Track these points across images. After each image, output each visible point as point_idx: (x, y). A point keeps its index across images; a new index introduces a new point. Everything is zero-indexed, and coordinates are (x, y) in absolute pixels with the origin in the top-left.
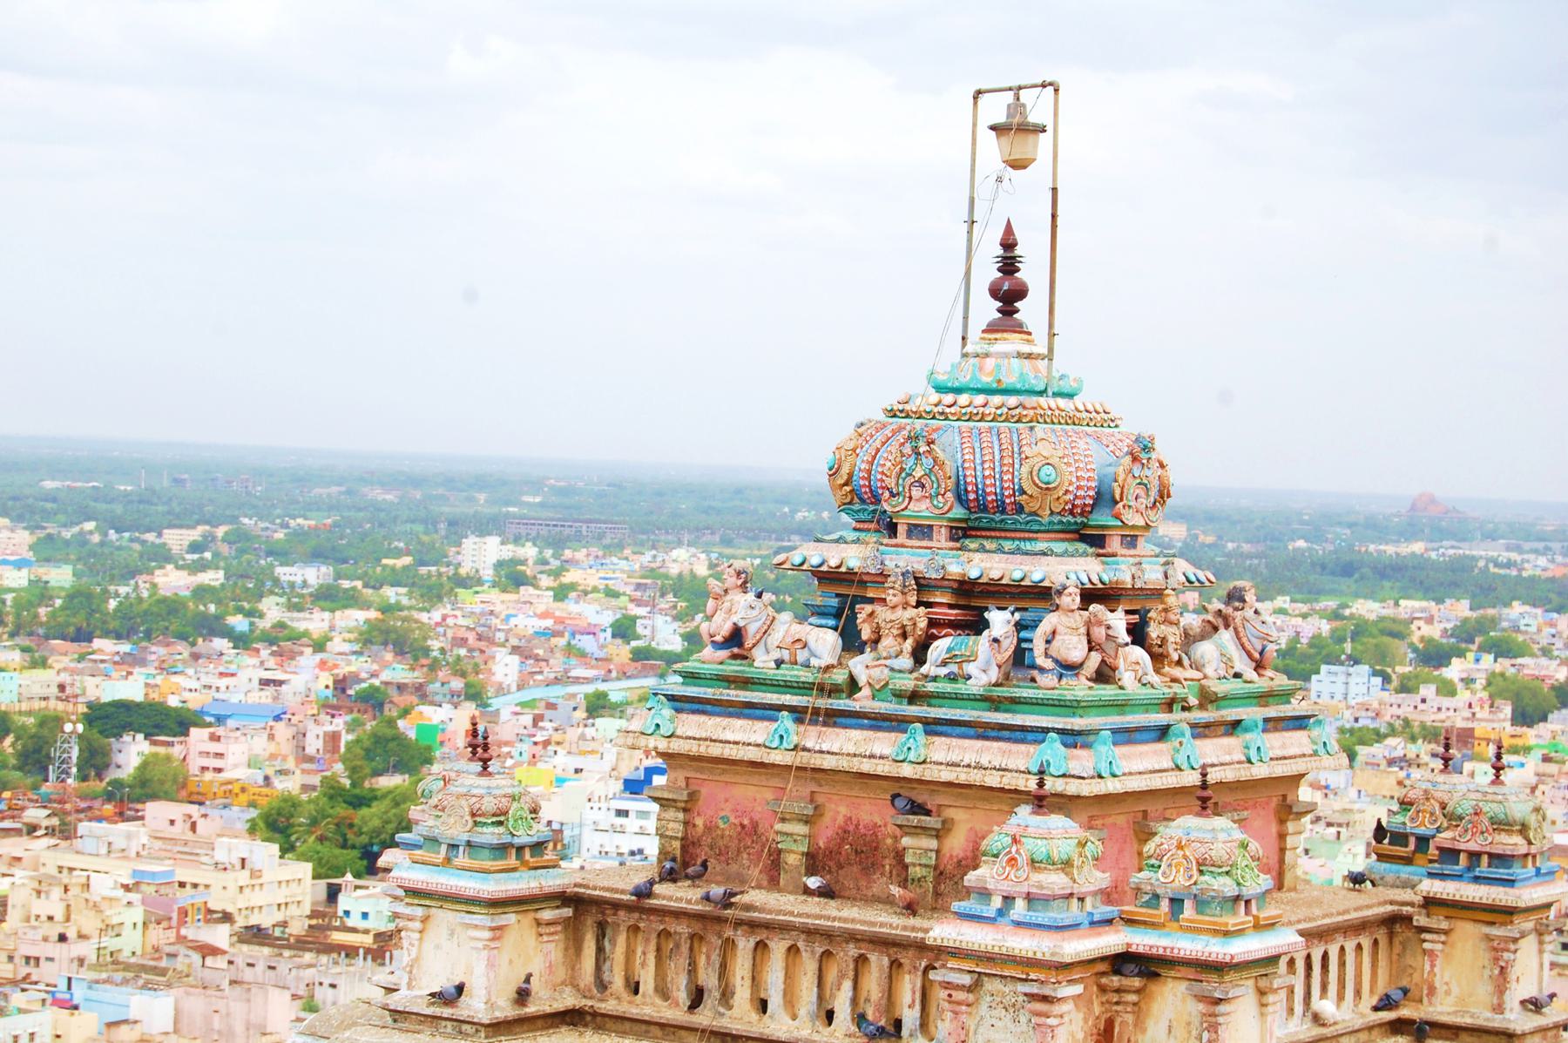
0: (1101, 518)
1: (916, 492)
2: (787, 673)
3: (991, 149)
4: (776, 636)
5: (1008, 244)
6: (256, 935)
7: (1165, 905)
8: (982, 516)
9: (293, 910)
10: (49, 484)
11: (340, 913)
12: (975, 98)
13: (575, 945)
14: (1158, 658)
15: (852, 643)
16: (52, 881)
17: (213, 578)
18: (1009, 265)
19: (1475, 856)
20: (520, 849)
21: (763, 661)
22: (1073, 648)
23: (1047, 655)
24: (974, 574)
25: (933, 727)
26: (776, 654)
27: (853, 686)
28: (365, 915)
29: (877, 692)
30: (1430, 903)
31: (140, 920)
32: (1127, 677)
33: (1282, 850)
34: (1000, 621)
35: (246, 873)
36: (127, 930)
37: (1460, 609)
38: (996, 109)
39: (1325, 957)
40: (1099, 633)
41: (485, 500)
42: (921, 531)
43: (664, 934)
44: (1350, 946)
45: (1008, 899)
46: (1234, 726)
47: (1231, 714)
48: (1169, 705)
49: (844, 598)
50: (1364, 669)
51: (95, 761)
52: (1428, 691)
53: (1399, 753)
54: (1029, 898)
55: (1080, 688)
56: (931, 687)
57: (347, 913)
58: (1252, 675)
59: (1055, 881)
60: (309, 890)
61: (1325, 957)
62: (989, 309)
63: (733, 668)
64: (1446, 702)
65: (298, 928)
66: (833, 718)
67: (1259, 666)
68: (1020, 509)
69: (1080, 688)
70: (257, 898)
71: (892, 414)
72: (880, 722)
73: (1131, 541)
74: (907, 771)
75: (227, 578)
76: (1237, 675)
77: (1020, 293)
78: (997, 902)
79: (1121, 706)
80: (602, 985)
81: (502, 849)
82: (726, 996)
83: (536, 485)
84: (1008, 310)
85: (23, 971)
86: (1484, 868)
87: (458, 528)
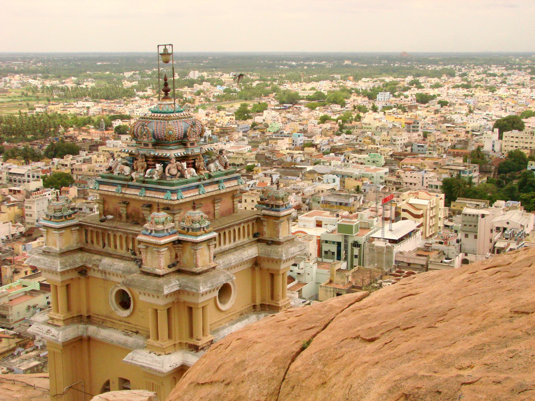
0: (185, 140)
1: (144, 137)
2: (120, 176)
4: (118, 168)
7: (186, 229)
8: (160, 142)
10: (99, 64)
13: (80, 234)
15: (133, 170)
19: (272, 205)
20: (65, 216)
21: (116, 173)
22: (174, 171)
23: (169, 173)
24: (156, 154)
25: (147, 189)
26: (118, 172)
27: (132, 179)
29: (137, 181)
30: (264, 215)
32: (188, 176)
33: (234, 205)
34: (158, 166)
37: (410, 78)
39: (239, 229)
40: (180, 168)
42: (146, 145)
43: (97, 232)
44: (246, 226)
45: (152, 231)
46: (217, 182)
47: (216, 179)
50: (388, 93)
52: (402, 97)
53: (396, 111)
56: (146, 180)
58: (224, 170)
59: (160, 227)
61: (239, 229)
63: (110, 175)
64: (406, 100)
66: (129, 186)
67: (225, 167)
68: (166, 140)
69: (175, 180)
71: (142, 118)
72: (139, 188)
73: (192, 144)
75: (139, 83)
76: (219, 170)
78: (149, 231)
80: (87, 242)
81: (61, 217)
82: (109, 245)
84: (166, 94)
85: (96, 173)
86: (274, 208)
87: (189, 69)
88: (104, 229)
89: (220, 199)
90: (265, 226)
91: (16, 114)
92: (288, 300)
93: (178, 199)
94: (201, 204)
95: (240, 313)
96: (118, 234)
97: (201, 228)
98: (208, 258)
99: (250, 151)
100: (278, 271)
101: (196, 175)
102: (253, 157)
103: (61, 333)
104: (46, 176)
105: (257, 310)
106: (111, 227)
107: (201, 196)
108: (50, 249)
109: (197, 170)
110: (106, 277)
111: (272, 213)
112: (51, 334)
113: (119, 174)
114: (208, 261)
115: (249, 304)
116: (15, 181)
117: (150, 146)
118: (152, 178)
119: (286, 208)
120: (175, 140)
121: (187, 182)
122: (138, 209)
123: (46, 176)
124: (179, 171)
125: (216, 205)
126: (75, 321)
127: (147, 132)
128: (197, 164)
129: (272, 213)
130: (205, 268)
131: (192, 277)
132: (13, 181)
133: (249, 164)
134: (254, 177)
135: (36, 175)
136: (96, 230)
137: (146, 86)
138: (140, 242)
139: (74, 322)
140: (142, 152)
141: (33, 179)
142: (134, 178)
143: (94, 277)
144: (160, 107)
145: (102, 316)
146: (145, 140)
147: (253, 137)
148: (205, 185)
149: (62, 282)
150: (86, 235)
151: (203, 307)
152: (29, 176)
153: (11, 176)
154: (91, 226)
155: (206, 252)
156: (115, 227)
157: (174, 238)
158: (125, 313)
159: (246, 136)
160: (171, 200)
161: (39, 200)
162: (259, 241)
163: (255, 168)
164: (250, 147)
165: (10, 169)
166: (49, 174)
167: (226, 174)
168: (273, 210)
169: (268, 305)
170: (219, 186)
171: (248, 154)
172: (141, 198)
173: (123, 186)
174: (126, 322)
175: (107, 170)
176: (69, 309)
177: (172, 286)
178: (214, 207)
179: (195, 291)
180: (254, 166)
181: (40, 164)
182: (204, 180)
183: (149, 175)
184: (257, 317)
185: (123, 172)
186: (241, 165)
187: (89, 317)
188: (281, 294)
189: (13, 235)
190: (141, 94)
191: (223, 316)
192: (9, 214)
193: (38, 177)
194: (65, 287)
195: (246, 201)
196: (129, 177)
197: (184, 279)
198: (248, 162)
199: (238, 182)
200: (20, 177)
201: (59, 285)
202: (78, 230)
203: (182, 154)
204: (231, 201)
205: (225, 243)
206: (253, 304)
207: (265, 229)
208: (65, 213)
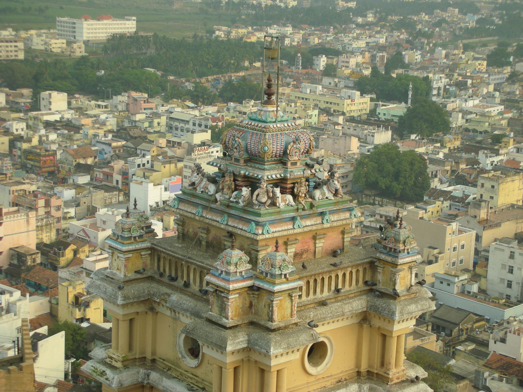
1: (235, 150)
4: (202, 184)
5: (135, 199)
6: (352, 120)
7: (264, 274)
11: (377, 114)
16: (292, 101)
20: (135, 237)
21: (199, 191)
25: (230, 215)
26: (202, 190)
27: (216, 201)
28: (384, 114)
31: (317, 114)
35: (350, 100)
36: (314, 117)
39: (344, 275)
42: (237, 160)
44: (354, 271)
45: (222, 272)
46: (322, 214)
51: (308, 63)
54: (226, 272)
56: (231, 204)
57: (379, 113)
60: (369, 106)
61: (344, 275)
65: (364, 117)
66: (212, 209)
70: (353, 108)
72: (222, 213)
76: (327, 198)
78: (220, 272)
81: (129, 238)
84: (269, 98)
88: (178, 258)
89: (324, 234)
90: (380, 273)
91: (189, 38)
92: (403, 370)
93: (263, 234)
94: (296, 239)
95: (337, 380)
96: (192, 267)
97: (281, 274)
98: (289, 311)
99: (501, 113)
100: (391, 332)
101: (293, 203)
102: (504, 122)
103: (116, 377)
104: (216, 126)
105: (363, 378)
106: (185, 256)
107: (296, 231)
108: (114, 274)
109: (295, 197)
110: (176, 315)
111: (389, 259)
112: (105, 377)
113: (202, 192)
114: (289, 315)
115: (351, 370)
116: (177, 129)
117: (242, 161)
118: (237, 202)
119: (408, 253)
120: (272, 157)
121: (279, 212)
122: (220, 238)
123: (216, 126)
124: (269, 197)
125: (317, 242)
126: (138, 364)
127: (238, 145)
128: (295, 190)
129: (389, 259)
130: (282, 325)
131: (265, 334)
132: (174, 129)
133: (496, 132)
134: (501, 152)
135: (203, 123)
136: (169, 258)
137: (367, 9)
138: (208, 283)
139: (135, 365)
140: (231, 169)
141: (200, 129)
142: (218, 199)
143: (163, 314)
144: (260, 114)
145: (168, 362)
146: (236, 155)
147: (509, 93)
148: (302, 217)
149: (124, 315)
150: (159, 261)
151: (278, 371)
152: (194, 124)
153: (172, 123)
154: (164, 252)
155: (287, 303)
156: (189, 258)
157: (249, 283)
158: (192, 362)
159: (499, 91)
160: (254, 234)
161: (203, 158)
162: (371, 290)
163: (505, 139)
164: (502, 107)
165: (172, 113)
166: (220, 124)
167: (336, 203)
168: (390, 255)
169: (377, 374)
170: (323, 219)
171: (497, 118)
172: (222, 226)
173: (205, 208)
174: (193, 374)
175: (190, 185)
176: (130, 347)
177: (239, 342)
178: (315, 244)
179: (264, 351)
180: (504, 136)
181: (211, 110)
182: (303, 209)
183: (235, 198)
184: (360, 387)
185: (207, 191)
186: (486, 132)
187: (154, 361)
188: (393, 361)
189: (164, 202)
190: (360, 20)
191: (312, 379)
192: (163, 173)
193: (206, 127)
194: (128, 322)
195: (483, 185)
196: (212, 199)
197: (256, 334)
198: (496, 129)
199: (351, 215)
200: (183, 125)
201: (121, 318)
202: (150, 254)
203: (278, 176)
204: (341, 236)
205: (322, 291)
206: (357, 370)
207: (380, 277)
208: (135, 234)
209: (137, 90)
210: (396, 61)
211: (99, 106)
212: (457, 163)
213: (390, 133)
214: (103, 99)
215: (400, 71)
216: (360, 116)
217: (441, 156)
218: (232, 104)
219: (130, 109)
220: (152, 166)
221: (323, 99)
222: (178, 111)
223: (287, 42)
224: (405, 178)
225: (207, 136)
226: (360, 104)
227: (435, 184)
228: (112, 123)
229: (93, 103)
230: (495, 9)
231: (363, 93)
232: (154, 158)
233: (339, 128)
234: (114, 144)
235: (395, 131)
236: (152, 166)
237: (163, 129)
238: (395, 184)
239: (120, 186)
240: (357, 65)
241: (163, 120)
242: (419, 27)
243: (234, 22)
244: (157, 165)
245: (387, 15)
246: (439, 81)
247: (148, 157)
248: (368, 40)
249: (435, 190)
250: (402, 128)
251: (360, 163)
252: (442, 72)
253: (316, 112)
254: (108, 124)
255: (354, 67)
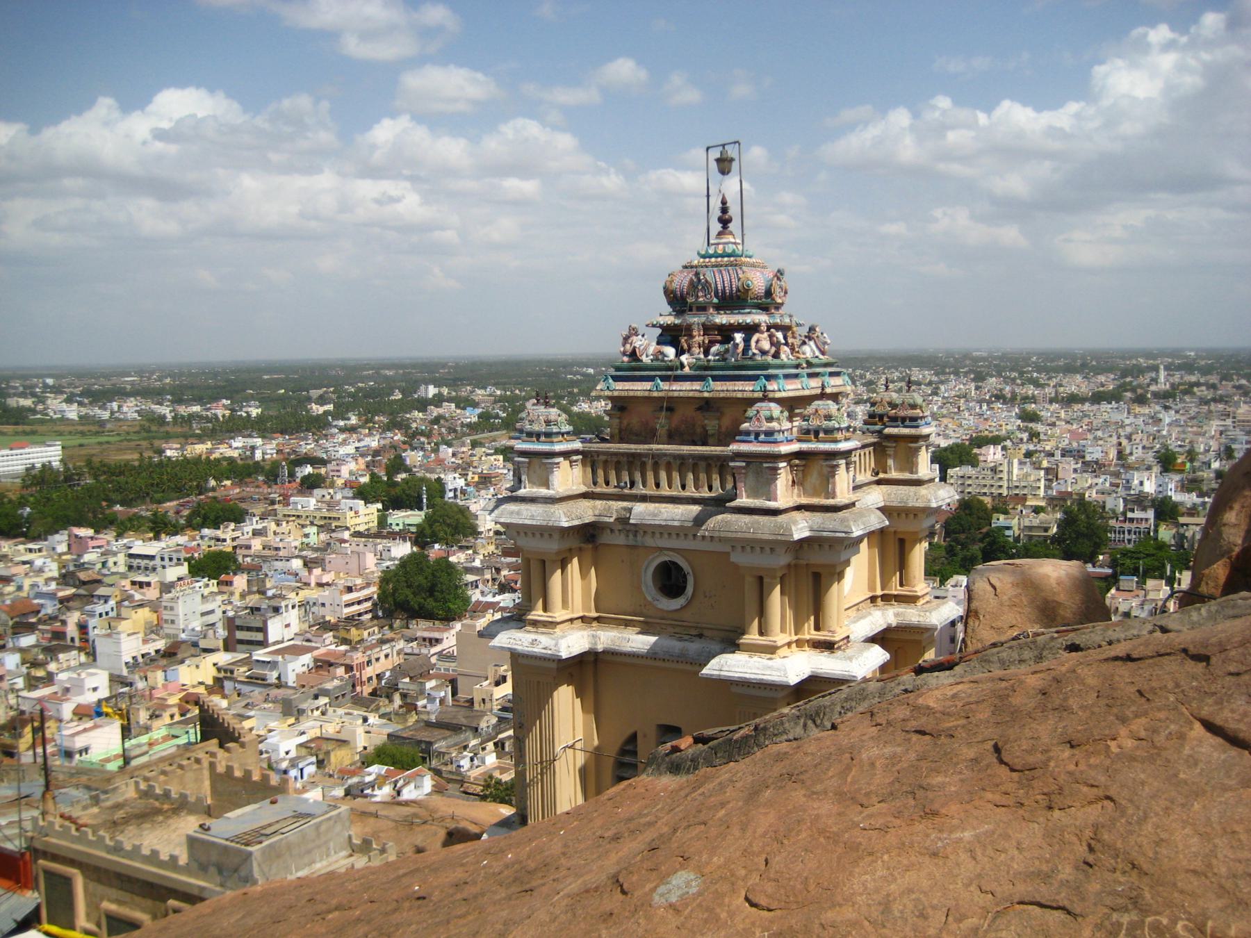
2: (655, 363)
3: (714, 166)
5: (724, 202)
6: (358, 534)
9: (371, 525)
12: (708, 149)
14: (793, 350)
17: (330, 407)
18: (724, 210)
27: (682, 366)
32: (783, 356)
38: (715, 154)
41: (431, 371)
48: (797, 366)
49: (670, 335)
55: (769, 359)
62: (719, 227)
70: (358, 521)
74: (706, 395)
77: (730, 220)
79: (783, 366)
83: (444, 366)
86: (907, 423)
104: (192, 558)
123: (192, 558)
124: (772, 344)
135: (175, 556)
137: (348, 411)
152: (162, 559)
173: (664, 379)
181: (180, 539)
190: (342, 423)
209: (79, 524)
210: (398, 465)
211: (31, 550)
212: (498, 570)
213: (408, 544)
214: (34, 539)
215: (404, 476)
216: (368, 530)
217: (477, 563)
218: (206, 531)
219: (77, 545)
220: (119, 615)
221: (318, 515)
222: (140, 547)
223: (258, 455)
224: (442, 592)
225: (184, 570)
226: (366, 515)
227: (476, 596)
228: (53, 570)
229: (21, 547)
230: (495, 402)
231: (367, 501)
232: (119, 604)
233: (347, 545)
234: (60, 594)
235: (415, 542)
236: (119, 615)
237: (122, 568)
238: (430, 600)
239: (77, 643)
240: (351, 473)
241: (121, 558)
242: (414, 425)
243: (187, 438)
244: (124, 612)
245: (373, 417)
246: (454, 481)
247: (112, 603)
248: (357, 445)
249: (478, 602)
250: (422, 538)
251: (386, 578)
252: (455, 470)
253: (314, 529)
254: (46, 569)
255: (347, 476)
